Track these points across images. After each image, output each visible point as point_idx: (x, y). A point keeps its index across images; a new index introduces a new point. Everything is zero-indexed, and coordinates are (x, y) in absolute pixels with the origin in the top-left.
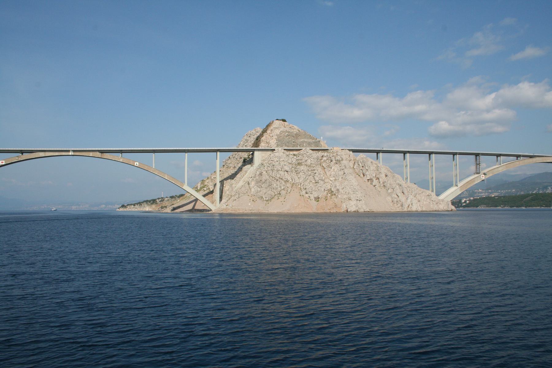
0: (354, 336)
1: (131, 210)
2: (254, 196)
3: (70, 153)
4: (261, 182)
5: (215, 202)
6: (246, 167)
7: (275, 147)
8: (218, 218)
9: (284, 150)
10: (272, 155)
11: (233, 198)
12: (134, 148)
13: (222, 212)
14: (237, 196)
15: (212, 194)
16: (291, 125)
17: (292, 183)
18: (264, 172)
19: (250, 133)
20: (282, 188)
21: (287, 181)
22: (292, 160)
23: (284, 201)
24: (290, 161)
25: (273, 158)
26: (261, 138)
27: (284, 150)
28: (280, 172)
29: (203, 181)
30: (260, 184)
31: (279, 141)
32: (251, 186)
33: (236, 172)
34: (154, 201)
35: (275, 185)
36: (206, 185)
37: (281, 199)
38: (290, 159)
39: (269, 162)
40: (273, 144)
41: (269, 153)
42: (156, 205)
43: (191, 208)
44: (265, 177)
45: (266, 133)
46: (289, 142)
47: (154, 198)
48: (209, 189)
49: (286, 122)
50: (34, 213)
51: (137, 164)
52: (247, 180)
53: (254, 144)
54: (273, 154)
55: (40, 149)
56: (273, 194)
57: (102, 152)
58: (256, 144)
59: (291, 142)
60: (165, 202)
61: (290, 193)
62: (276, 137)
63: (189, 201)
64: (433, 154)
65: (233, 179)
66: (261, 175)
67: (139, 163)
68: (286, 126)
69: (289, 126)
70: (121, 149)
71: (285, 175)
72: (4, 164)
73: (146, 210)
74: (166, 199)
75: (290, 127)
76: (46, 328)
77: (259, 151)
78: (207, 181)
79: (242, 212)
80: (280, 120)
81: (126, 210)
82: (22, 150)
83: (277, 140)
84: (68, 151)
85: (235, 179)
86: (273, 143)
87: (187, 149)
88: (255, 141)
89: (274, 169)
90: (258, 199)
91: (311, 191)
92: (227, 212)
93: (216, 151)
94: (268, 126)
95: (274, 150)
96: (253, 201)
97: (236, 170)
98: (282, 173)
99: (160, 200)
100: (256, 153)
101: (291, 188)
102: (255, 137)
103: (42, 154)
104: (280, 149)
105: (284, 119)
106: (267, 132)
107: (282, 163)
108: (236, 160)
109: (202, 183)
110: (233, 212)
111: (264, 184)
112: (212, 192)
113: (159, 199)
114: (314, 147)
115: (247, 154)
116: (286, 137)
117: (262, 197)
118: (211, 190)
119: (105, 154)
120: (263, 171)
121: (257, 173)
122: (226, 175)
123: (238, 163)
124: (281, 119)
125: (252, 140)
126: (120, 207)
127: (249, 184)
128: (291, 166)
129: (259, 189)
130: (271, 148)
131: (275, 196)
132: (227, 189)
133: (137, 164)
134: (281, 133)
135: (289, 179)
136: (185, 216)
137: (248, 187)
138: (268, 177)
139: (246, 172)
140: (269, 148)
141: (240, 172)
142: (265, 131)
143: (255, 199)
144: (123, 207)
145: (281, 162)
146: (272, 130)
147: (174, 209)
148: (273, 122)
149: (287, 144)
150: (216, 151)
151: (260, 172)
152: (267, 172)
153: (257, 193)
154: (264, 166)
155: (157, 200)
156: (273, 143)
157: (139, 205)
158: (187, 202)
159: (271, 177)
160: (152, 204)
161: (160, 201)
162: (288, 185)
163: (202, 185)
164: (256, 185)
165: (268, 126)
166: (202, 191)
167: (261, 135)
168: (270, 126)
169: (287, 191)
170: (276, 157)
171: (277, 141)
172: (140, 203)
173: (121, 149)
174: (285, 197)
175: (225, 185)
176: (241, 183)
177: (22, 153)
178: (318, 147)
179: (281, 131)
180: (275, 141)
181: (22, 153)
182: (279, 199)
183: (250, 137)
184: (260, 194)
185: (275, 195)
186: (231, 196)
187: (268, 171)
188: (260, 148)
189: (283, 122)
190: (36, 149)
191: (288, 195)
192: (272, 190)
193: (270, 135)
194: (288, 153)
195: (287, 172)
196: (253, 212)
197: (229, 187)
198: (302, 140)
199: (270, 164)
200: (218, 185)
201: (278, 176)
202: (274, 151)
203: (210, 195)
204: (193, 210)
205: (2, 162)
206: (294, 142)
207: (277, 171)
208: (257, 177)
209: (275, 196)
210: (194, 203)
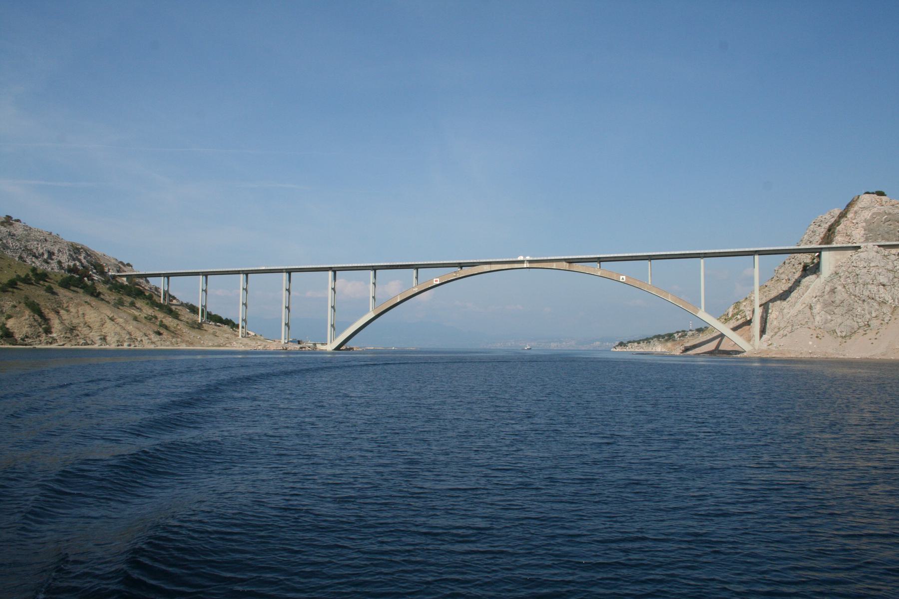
1: (633, 350)
2: (820, 328)
3: (525, 265)
4: (834, 305)
5: (753, 339)
6: (807, 278)
7: (862, 242)
8: (756, 367)
9: (879, 246)
10: (854, 257)
11: (782, 332)
13: (759, 355)
14: (789, 329)
15: (749, 325)
16: (893, 202)
17: (893, 306)
18: (840, 288)
19: (820, 218)
20: (874, 315)
21: (884, 302)
22: (895, 265)
23: (876, 339)
24: (890, 267)
25: (856, 263)
26: (835, 229)
27: (879, 246)
28: (869, 286)
29: (738, 304)
30: (831, 308)
31: (869, 231)
32: (815, 311)
33: (791, 287)
34: (670, 337)
35: (859, 309)
36: (741, 311)
37: (871, 334)
38: (890, 263)
39: (850, 270)
40: (858, 237)
41: (850, 253)
42: (673, 343)
43: (713, 349)
44: (841, 295)
45: (846, 219)
46: (891, 232)
47: (671, 332)
48: (745, 316)
49: (885, 195)
51: (623, 279)
52: (808, 301)
53: (823, 239)
54: (856, 255)
55: (484, 261)
56: (856, 326)
57: (570, 261)
58: (828, 238)
59: (893, 232)
60: (689, 338)
61: (887, 323)
62: (864, 224)
63: (711, 337)
64: (756, 254)
65: (785, 300)
66: (834, 292)
67: (626, 277)
68: (884, 203)
69: (891, 204)
70: (598, 256)
71: (879, 291)
72: (438, 283)
73: (657, 350)
74: (690, 333)
75: (893, 205)
76: (251, 529)
77: (829, 251)
78: (744, 304)
79: (794, 356)
80: (873, 193)
81: (625, 350)
82: (460, 263)
83: (865, 230)
84: (522, 262)
85: (788, 299)
86: (858, 235)
87: (702, 252)
88: (826, 234)
89: (858, 282)
90: (827, 335)
92: (768, 356)
94: (849, 205)
95: (859, 247)
96: (817, 337)
97: (790, 285)
98: (874, 288)
99: (680, 334)
100: (825, 254)
101: (892, 314)
102: (827, 226)
103: (486, 268)
104: (870, 245)
105: (880, 190)
106: (846, 217)
107: (874, 271)
108: (792, 268)
109: (735, 307)
110: (778, 356)
111: (838, 308)
112: (749, 322)
113: (678, 332)
115: (810, 256)
116: (884, 223)
117: (834, 331)
118: (748, 319)
119: (574, 264)
120: (836, 286)
121: (826, 290)
122: (774, 294)
123: (794, 273)
124: (874, 191)
125: (822, 231)
126: (617, 346)
127: (811, 308)
128: (891, 275)
129: (829, 317)
130: (855, 245)
131: (858, 329)
132: (775, 317)
133: (623, 278)
134: (874, 216)
135: (887, 299)
136: (701, 361)
137: (810, 314)
138: (845, 296)
139: (808, 287)
140: (850, 245)
141: (798, 288)
142: (843, 215)
143: (822, 335)
144: (621, 346)
145: (872, 268)
146: (856, 212)
147: (687, 349)
148: (858, 198)
149: (886, 236)
151: (831, 286)
152: (844, 287)
153: (825, 323)
154: (840, 277)
155: (676, 335)
156: (858, 235)
157: (646, 342)
158: (709, 338)
159: (853, 295)
160: (667, 341)
161: (680, 337)
162: (886, 309)
163: (736, 311)
164: (825, 310)
165: (849, 205)
166: (734, 321)
167: (837, 222)
168: (853, 206)
169: (883, 320)
170: (861, 260)
171: (867, 232)
172: (648, 340)
173: (598, 256)
174: (877, 331)
175: (770, 311)
176: (799, 307)
177: (461, 267)
179: (874, 214)
180: (863, 232)
181: (461, 267)
182: (865, 334)
183: (819, 226)
184: (830, 326)
185: (860, 327)
186: (779, 329)
187: (848, 284)
188: (834, 245)
189: (878, 197)
190: (478, 261)
191: (884, 327)
192: (855, 318)
193: (854, 221)
194: (886, 252)
195: (884, 285)
196: (815, 356)
197: (777, 313)
199: (850, 273)
200: (759, 311)
201: (866, 293)
202: (859, 250)
203: (746, 327)
204: (716, 352)
205: (436, 281)
207: (864, 285)
208: (826, 297)
209: (858, 329)
210: (718, 340)
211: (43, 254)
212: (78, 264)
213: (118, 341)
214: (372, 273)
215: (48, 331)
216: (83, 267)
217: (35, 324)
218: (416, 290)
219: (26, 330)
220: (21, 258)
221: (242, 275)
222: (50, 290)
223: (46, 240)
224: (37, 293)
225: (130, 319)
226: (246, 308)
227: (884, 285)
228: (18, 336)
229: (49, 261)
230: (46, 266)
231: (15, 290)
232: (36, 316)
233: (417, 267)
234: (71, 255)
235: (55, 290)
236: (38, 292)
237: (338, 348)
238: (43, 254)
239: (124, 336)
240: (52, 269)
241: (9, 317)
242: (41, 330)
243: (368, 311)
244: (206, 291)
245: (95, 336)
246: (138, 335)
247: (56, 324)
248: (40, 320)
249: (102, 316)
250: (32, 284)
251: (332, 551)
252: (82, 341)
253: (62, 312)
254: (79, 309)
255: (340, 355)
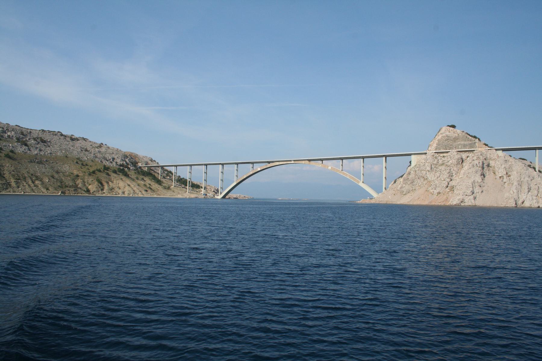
0: (390, 313)
3: (292, 162)
12: (539, 145)
50: (258, 200)
68: (451, 131)
84: (291, 161)
91: (435, 187)
93: (535, 149)
103: (278, 163)
105: (453, 124)
114: (469, 149)
150: (535, 149)
178: (473, 148)
195: (429, 171)
198: (459, 143)
206: (451, 145)
211: (110, 159)
212: (124, 162)
213: (128, 194)
214: (341, 161)
215: (102, 190)
216: (127, 164)
217: (98, 187)
218: (251, 173)
219: (95, 189)
220: (101, 161)
221: (220, 165)
222: (108, 174)
223: (113, 153)
224: (102, 176)
225: (136, 185)
226: (206, 182)
227: (429, 171)
228: (91, 191)
229: (113, 162)
230: (111, 164)
231: (94, 175)
232: (99, 184)
233: (253, 163)
234: (122, 159)
235: (110, 174)
236: (103, 175)
237: (224, 197)
238: (110, 159)
239: (131, 191)
240: (113, 165)
241: (90, 184)
242: (100, 189)
243: (233, 182)
244: (237, 170)
245: (120, 192)
246: (137, 191)
247: (106, 187)
248: (100, 186)
249: (125, 184)
250: (102, 172)
251: (367, 335)
252: (115, 193)
253: (110, 183)
254: (117, 181)
255: (225, 200)
